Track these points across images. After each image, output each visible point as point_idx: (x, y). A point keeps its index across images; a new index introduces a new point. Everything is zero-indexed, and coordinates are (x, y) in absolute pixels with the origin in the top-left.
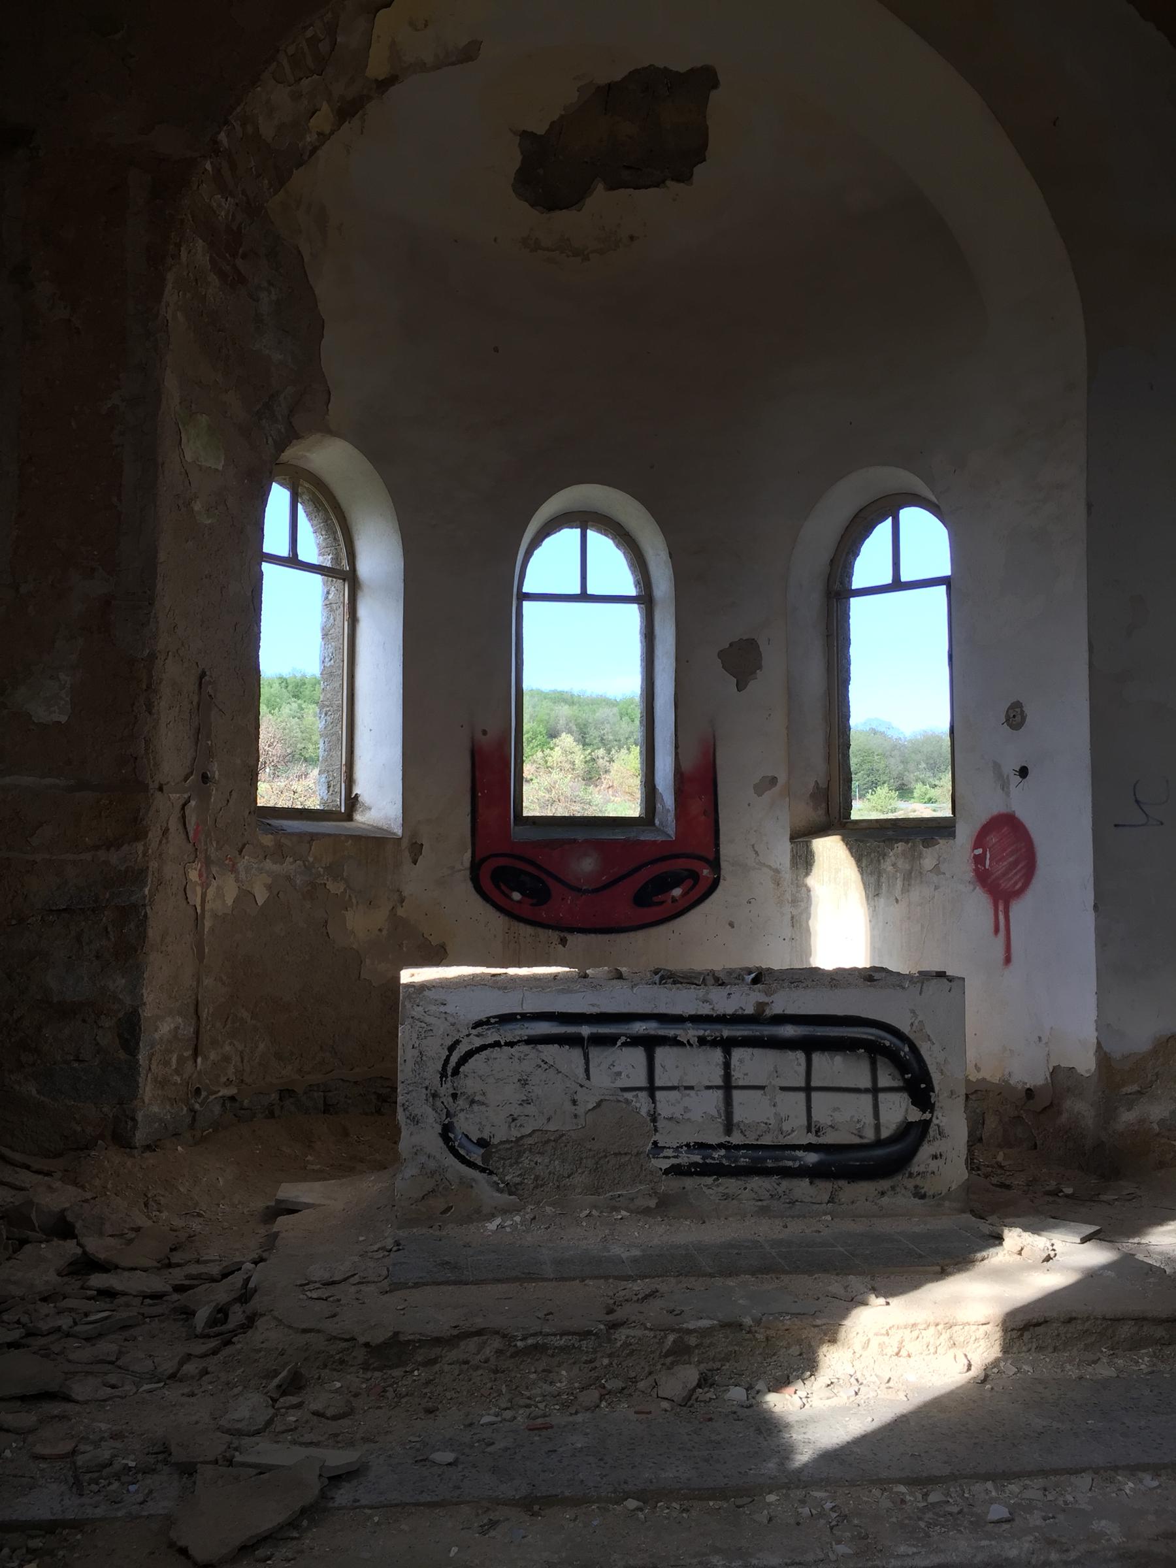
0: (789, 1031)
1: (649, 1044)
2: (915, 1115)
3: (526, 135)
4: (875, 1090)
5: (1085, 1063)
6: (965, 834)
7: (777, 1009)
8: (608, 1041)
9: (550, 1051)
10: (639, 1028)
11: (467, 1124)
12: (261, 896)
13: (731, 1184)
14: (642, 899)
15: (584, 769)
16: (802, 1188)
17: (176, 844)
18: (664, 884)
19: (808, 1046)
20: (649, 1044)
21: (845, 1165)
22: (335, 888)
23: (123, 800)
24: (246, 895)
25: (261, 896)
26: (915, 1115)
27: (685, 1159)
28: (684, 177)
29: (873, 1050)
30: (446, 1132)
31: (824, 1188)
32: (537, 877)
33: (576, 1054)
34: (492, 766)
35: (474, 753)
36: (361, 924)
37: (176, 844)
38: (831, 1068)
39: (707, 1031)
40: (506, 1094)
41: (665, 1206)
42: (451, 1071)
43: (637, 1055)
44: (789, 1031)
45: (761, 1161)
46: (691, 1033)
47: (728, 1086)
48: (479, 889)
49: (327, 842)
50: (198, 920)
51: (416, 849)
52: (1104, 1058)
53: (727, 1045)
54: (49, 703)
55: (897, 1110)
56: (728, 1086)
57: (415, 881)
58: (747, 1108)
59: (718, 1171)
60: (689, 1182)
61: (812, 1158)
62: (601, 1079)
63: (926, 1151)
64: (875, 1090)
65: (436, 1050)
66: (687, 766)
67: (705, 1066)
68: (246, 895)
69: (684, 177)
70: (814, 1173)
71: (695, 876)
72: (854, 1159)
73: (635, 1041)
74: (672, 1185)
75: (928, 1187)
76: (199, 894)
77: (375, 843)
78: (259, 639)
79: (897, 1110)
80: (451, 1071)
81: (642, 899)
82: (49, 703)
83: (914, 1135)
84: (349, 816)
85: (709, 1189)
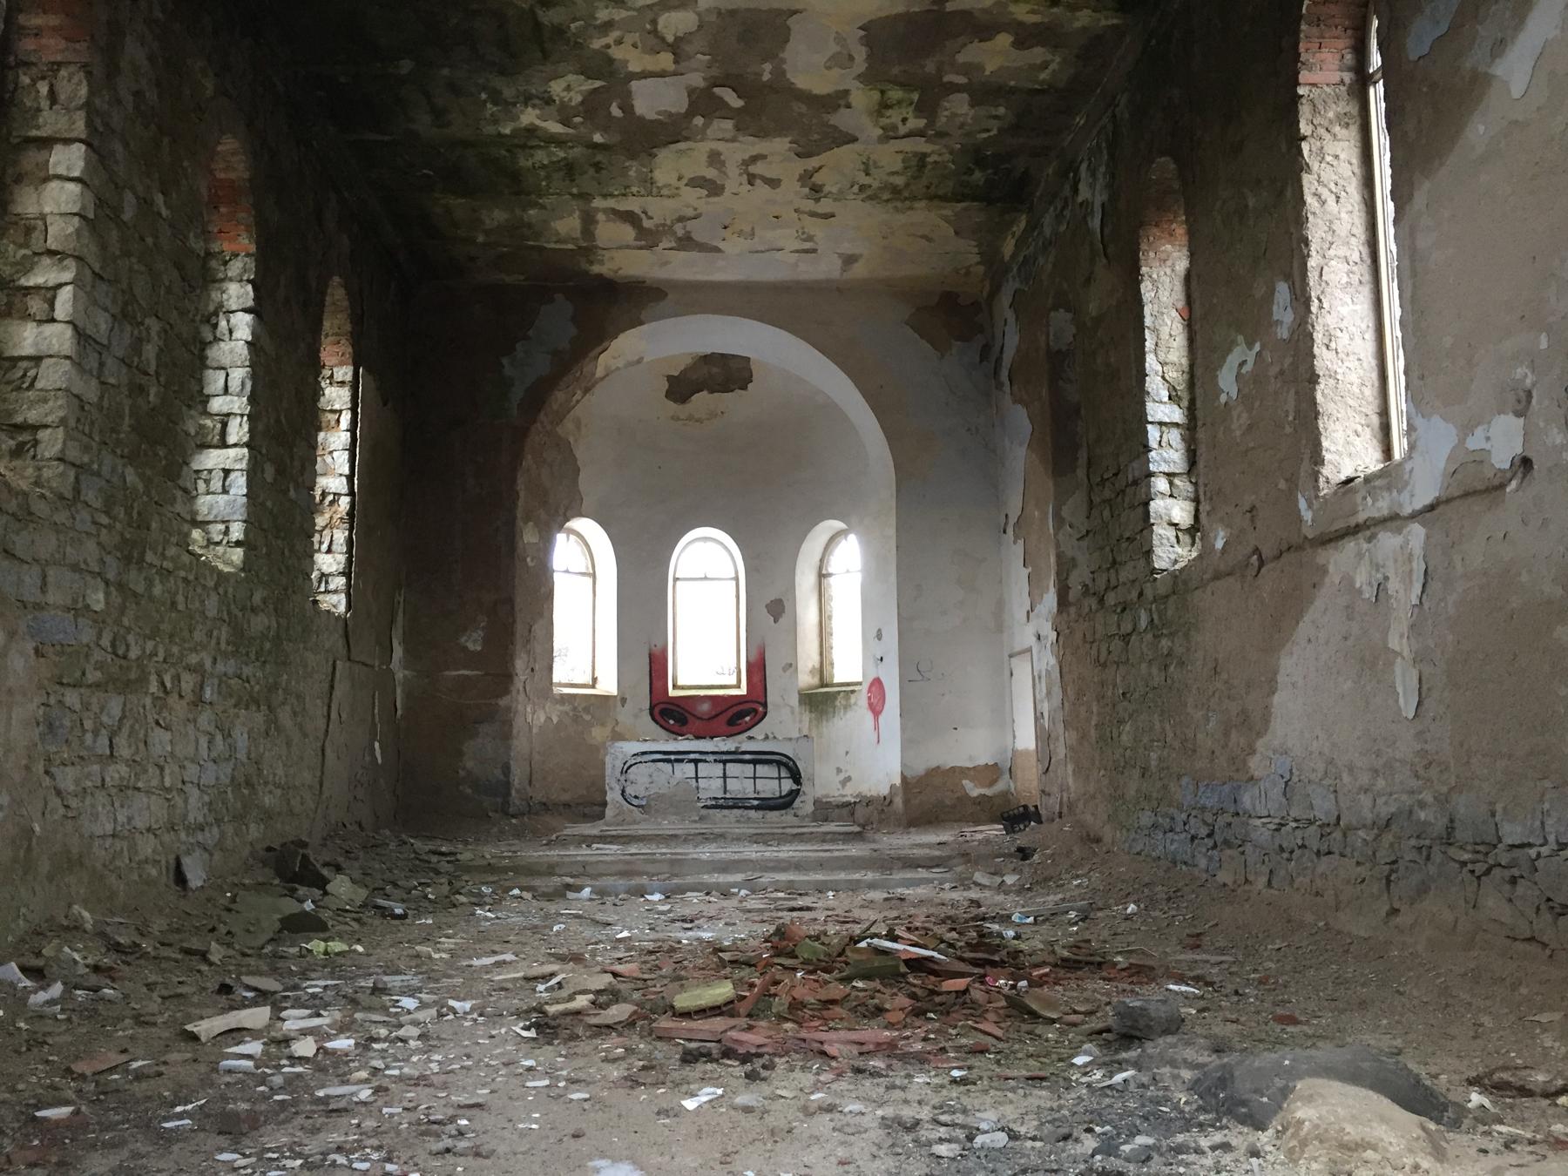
0: (747, 757)
1: (696, 762)
2: (795, 787)
3: (670, 378)
4: (780, 778)
5: (898, 781)
6: (865, 687)
7: (743, 749)
8: (681, 761)
9: (660, 764)
10: (692, 756)
11: (630, 791)
12: (555, 720)
13: (726, 812)
14: (731, 722)
15: (706, 658)
16: (752, 813)
17: (521, 697)
18: (741, 715)
19: (755, 762)
20: (696, 762)
21: (767, 805)
22: (587, 718)
23: (503, 679)
24: (549, 719)
25: (555, 720)
26: (795, 787)
27: (709, 803)
28: (744, 388)
29: (779, 764)
30: (623, 792)
31: (761, 813)
32: (674, 713)
33: (668, 766)
34: (657, 665)
35: (650, 656)
36: (598, 734)
37: (521, 697)
38: (762, 770)
39: (717, 757)
40: (643, 780)
41: (702, 819)
42: (624, 772)
43: (692, 766)
44: (747, 757)
45: (737, 804)
46: (711, 758)
47: (725, 777)
48: (654, 719)
49: (589, 708)
50: (530, 728)
51: (624, 701)
52: (904, 778)
53: (725, 762)
54: (473, 642)
55: (788, 785)
56: (725, 777)
57: (624, 716)
58: (733, 785)
59: (721, 807)
60: (711, 811)
61: (756, 803)
62: (678, 774)
63: (798, 800)
64: (780, 778)
65: (619, 765)
66: (752, 659)
67: (718, 769)
68: (549, 719)
69: (744, 388)
70: (757, 808)
71: (756, 711)
72: (771, 803)
73: (690, 761)
74: (704, 812)
75: (800, 813)
76: (532, 718)
77: (605, 699)
78: (549, 596)
79: (788, 785)
80: (624, 772)
81: (731, 722)
82: (473, 642)
83: (794, 794)
84: (593, 686)
85: (718, 813)
